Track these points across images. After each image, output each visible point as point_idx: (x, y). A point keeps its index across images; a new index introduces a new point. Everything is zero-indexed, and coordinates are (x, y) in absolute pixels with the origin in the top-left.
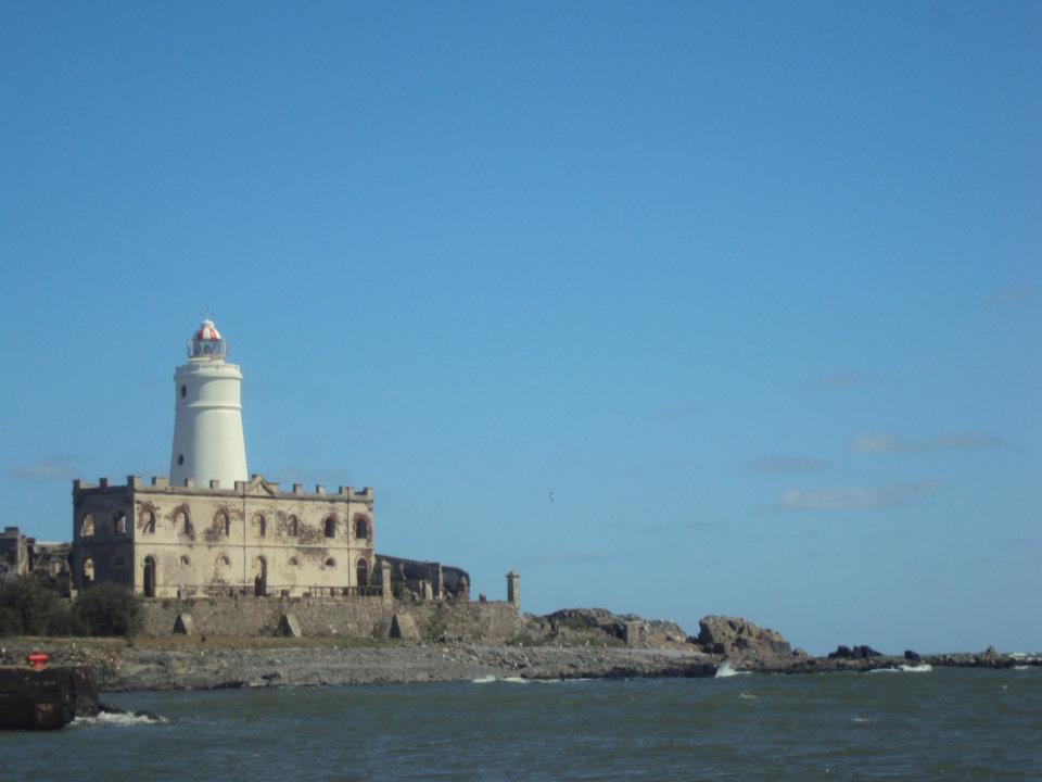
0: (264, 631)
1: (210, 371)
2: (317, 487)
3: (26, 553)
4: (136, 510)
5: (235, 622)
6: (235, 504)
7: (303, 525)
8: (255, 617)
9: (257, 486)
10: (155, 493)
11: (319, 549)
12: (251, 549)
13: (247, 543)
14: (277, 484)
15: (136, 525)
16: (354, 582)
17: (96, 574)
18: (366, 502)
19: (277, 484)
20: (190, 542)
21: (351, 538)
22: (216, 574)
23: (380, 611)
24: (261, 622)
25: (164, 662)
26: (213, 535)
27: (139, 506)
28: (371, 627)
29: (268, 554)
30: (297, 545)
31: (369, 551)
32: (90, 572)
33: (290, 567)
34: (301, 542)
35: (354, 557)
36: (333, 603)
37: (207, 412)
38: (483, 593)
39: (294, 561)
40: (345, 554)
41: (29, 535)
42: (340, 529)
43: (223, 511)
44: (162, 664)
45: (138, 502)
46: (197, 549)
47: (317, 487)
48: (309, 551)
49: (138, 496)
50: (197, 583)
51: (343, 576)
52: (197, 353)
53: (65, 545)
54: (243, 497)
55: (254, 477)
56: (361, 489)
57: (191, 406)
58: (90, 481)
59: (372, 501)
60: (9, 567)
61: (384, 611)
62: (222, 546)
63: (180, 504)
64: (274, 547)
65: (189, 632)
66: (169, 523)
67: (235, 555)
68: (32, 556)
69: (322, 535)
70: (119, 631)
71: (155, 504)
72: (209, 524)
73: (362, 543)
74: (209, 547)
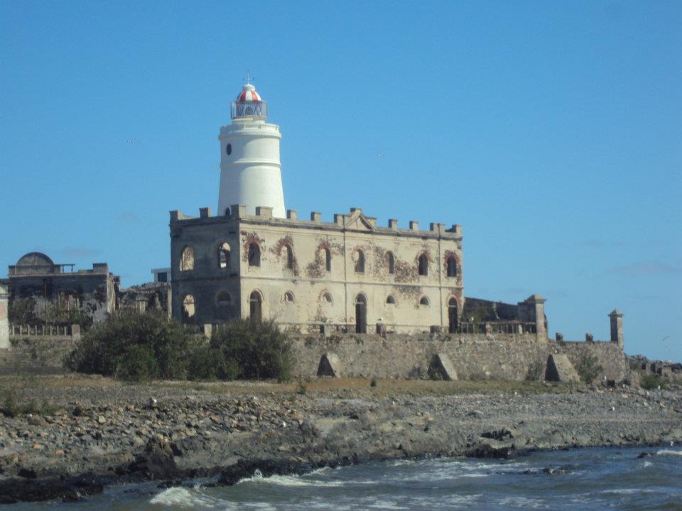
0: (416, 373)
1: (253, 130)
2: (411, 223)
3: (113, 291)
4: (241, 242)
5: (385, 363)
6: (335, 238)
7: (398, 261)
8: (405, 356)
9: (356, 221)
10: (259, 224)
11: (414, 287)
12: (351, 285)
13: (348, 280)
14: (374, 219)
15: (241, 259)
16: (446, 322)
17: (197, 309)
18: (455, 240)
19: (374, 219)
20: (294, 278)
21: (443, 275)
22: (319, 312)
23: (535, 349)
24: (411, 363)
25: (358, 415)
26: (314, 270)
27: (244, 236)
28: (526, 369)
29: (368, 291)
30: (393, 282)
31: (459, 289)
32: (191, 309)
33: (387, 305)
34: (398, 279)
35: (446, 295)
36: (487, 341)
37: (252, 168)
38: (590, 333)
39: (390, 300)
40: (437, 288)
41: (116, 274)
42: (433, 267)
43: (325, 246)
44: (356, 417)
45: (244, 233)
46: (301, 285)
47: (411, 223)
48: (405, 289)
49: (243, 227)
50: (300, 321)
51: (437, 315)
52: (240, 114)
53: (151, 283)
54: (344, 231)
55: (353, 210)
56: (450, 227)
57: (236, 162)
58: (189, 212)
59: (460, 239)
60: (98, 305)
61: (539, 351)
62: (324, 282)
63: (284, 237)
64: (373, 284)
65: (338, 375)
66: (272, 256)
67: (337, 292)
68: (119, 294)
69: (416, 272)
70: (266, 375)
71: (260, 236)
72: (311, 259)
73: (452, 282)
74: (313, 283)
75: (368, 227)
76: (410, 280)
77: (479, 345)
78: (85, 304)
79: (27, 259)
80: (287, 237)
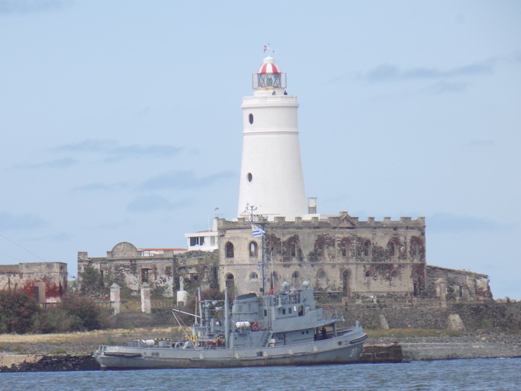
11: (387, 265)
20: (299, 262)
33: (367, 278)
74: (313, 266)
75: (352, 224)
76: (384, 260)
77: (404, 309)
78: (158, 277)
79: (118, 247)
80: (295, 235)
